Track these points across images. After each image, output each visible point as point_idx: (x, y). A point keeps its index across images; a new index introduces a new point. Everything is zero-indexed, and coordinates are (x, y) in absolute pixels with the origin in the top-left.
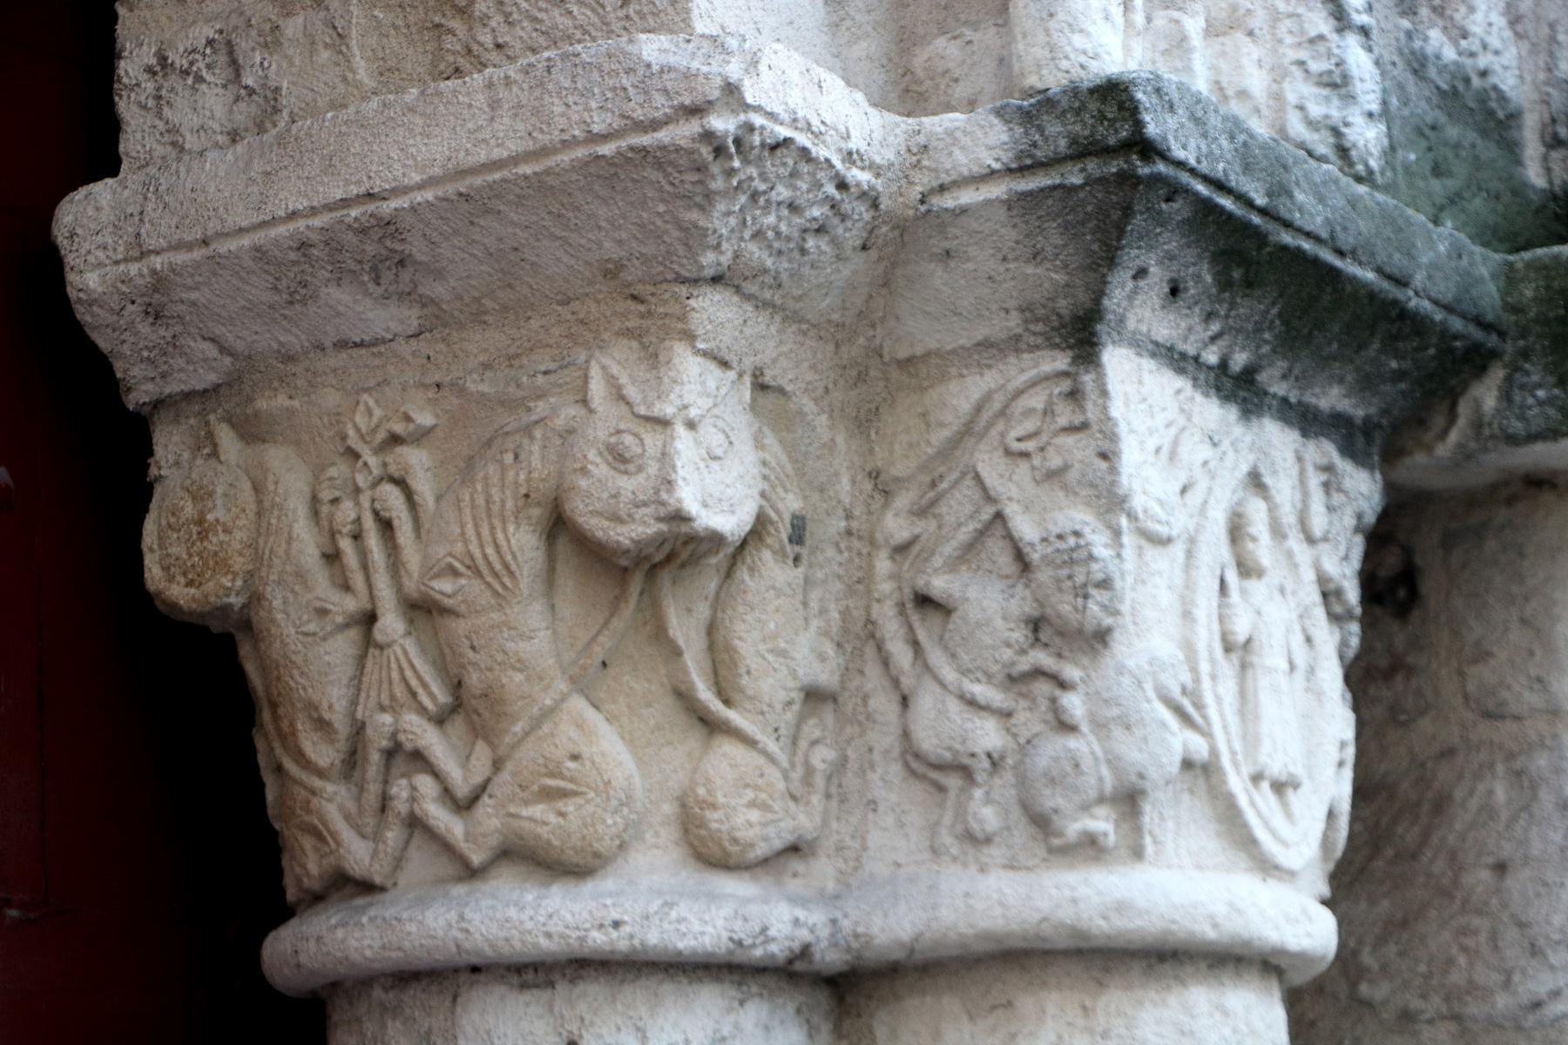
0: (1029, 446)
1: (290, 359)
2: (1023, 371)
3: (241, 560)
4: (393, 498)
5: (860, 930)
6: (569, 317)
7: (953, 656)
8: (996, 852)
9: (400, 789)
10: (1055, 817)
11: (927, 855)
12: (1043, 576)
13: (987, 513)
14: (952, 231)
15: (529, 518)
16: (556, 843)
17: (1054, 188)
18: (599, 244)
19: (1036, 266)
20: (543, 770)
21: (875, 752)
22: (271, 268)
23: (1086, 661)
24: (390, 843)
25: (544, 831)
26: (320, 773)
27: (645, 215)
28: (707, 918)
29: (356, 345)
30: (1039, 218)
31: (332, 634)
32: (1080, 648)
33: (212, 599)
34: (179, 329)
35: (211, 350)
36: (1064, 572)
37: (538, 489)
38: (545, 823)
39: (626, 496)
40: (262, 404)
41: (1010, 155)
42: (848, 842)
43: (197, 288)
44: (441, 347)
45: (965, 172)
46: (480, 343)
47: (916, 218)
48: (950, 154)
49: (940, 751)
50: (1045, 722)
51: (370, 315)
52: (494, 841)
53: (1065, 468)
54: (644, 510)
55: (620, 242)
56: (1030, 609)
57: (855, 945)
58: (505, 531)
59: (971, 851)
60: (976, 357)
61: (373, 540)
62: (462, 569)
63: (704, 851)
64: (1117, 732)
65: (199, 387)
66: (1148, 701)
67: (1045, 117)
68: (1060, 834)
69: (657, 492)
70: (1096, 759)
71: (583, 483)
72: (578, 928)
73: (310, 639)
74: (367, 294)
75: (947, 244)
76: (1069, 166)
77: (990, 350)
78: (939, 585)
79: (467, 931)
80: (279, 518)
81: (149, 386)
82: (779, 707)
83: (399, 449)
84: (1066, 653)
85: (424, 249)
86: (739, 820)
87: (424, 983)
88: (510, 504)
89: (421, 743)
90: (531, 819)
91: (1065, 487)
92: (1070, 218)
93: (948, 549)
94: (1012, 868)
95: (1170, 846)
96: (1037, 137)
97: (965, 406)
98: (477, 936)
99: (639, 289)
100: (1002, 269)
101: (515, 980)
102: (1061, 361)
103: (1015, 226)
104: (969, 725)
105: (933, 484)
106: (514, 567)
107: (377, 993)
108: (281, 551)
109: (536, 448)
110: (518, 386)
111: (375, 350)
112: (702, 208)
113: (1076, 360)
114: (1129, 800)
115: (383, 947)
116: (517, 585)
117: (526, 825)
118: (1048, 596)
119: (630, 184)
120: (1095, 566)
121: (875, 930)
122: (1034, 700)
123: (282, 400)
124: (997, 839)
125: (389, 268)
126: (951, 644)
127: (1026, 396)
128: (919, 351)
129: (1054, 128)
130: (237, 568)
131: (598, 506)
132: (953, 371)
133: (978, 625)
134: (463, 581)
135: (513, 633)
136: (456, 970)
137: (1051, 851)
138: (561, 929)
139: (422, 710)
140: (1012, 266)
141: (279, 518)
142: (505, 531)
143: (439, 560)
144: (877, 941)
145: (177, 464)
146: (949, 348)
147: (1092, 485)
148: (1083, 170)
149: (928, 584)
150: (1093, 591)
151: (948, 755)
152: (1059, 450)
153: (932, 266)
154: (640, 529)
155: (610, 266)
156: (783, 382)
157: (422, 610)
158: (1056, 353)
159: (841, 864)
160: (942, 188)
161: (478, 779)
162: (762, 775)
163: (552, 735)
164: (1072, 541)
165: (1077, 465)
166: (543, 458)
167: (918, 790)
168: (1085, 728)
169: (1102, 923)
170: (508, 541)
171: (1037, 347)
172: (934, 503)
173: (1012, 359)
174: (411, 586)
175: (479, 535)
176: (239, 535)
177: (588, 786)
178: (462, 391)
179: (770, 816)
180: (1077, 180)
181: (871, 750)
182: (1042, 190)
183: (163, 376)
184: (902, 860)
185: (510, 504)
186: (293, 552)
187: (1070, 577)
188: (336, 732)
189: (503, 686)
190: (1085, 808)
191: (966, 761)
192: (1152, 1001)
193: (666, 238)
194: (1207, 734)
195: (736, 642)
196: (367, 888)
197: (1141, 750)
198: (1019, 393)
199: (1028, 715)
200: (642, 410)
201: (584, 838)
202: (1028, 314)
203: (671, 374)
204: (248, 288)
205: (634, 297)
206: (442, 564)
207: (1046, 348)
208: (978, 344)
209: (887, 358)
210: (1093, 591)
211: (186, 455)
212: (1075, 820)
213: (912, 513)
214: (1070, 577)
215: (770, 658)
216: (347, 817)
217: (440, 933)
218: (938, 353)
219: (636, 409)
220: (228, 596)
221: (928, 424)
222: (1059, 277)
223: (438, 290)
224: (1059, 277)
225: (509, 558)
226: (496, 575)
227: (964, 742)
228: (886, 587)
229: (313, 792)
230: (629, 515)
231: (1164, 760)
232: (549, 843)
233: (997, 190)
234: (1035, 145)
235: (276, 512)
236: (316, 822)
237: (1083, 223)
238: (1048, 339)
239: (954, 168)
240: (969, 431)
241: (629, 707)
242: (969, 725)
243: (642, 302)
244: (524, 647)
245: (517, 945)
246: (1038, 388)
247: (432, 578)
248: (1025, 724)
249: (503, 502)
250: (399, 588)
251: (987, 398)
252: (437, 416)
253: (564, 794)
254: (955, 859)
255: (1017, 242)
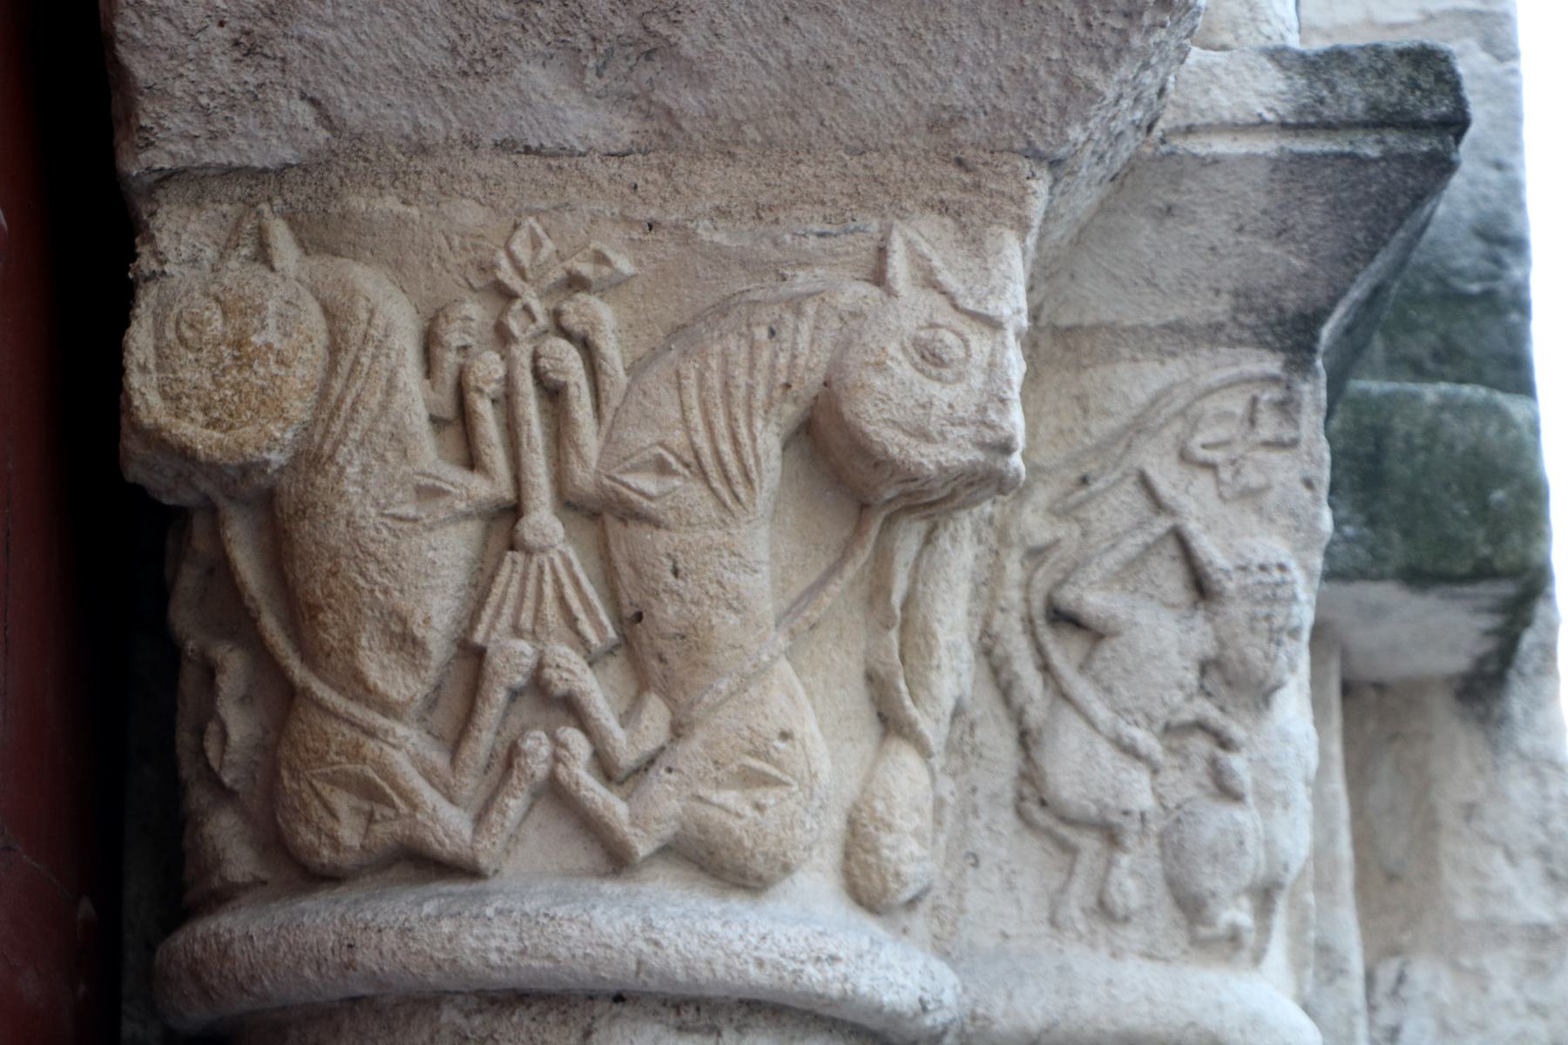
0: (1217, 456)
1: (423, 150)
2: (1216, 367)
3: (298, 404)
4: (568, 362)
5: (980, 1010)
6: (861, 171)
7: (1108, 690)
8: (1132, 935)
9: (537, 746)
10: (1211, 902)
11: (1045, 929)
12: (1237, 611)
13: (1162, 525)
14: (1188, 183)
15: (779, 415)
16: (748, 843)
17: (1341, 156)
18: (946, 83)
19: (1276, 246)
20: (747, 746)
21: (979, 794)
22: (462, 21)
23: (1248, 721)
24: (511, 814)
25: (735, 824)
26: (387, 708)
27: (1028, 58)
29: (527, 150)
30: (1306, 188)
31: (443, 523)
32: (1246, 706)
33: (249, 450)
34: (275, 75)
35: (305, 114)
36: (1263, 610)
37: (802, 380)
38: (739, 816)
39: (940, 408)
40: (357, 202)
41: (1288, 106)
42: (946, 901)
43: (334, 26)
44: (654, 175)
45: (1227, 116)
46: (714, 181)
47: (1153, 159)
48: (1207, 92)
49: (1085, 802)
50: (1200, 786)
51: (570, 114)
52: (667, 831)
53: (1267, 488)
54: (963, 431)
55: (975, 87)
56: (1209, 648)
57: (970, 1029)
58: (750, 426)
59: (1101, 929)
60: (1158, 340)
61: (531, 408)
62: (676, 465)
63: (861, 882)
65: (257, 164)
67: (1337, 72)
68: (1210, 923)
69: (982, 409)
71: (878, 382)
72: (794, 959)
73: (406, 526)
74: (580, 85)
75: (1173, 198)
76: (1359, 134)
77: (1181, 336)
78: (1093, 600)
79: (657, 943)
80: (374, 358)
81: (183, 148)
83: (582, 297)
84: (1230, 708)
85: (701, 41)
87: (535, 1009)
88: (761, 392)
89: (577, 686)
90: (721, 807)
91: (1259, 511)
92: (1344, 195)
93: (1111, 561)
94: (1150, 957)
96: (1325, 93)
97: (1140, 397)
98: (671, 951)
99: (969, 153)
100: (1231, 240)
101: (672, 1019)
102: (1272, 364)
103: (1270, 192)
104: (1123, 776)
105: (1084, 481)
106: (754, 475)
107: (449, 1015)
108: (374, 402)
109: (805, 327)
110: (776, 244)
111: (554, 163)
112: (1104, 67)
113: (1288, 365)
115: (523, 952)
116: (752, 500)
117: (716, 814)
118: (1235, 635)
119: (1031, 14)
121: (997, 1013)
122: (1187, 758)
123: (391, 203)
124: (1135, 919)
125: (627, 58)
126: (1105, 675)
127: (1215, 397)
128: (1089, 319)
129: (1348, 87)
130: (292, 413)
131: (898, 416)
132: (1125, 352)
133: (1150, 657)
134: (677, 482)
135: (735, 560)
136: (591, 997)
137: (1196, 942)
138: (776, 956)
139: (581, 641)
140: (1244, 239)
141: (374, 358)
142: (750, 426)
143: (642, 449)
144: (996, 1027)
145: (194, 261)
146: (1127, 323)
147: (1293, 514)
148: (1381, 142)
149: (1079, 599)
151: (1093, 809)
152: (1259, 467)
153: (1142, 221)
154: (953, 454)
155: (946, 116)
157: (599, 513)
158: (1264, 353)
159: (935, 926)
160: (1190, 130)
161: (649, 746)
163: (762, 702)
164: (1277, 575)
165: (1278, 489)
166: (813, 341)
167: (1033, 848)
168: (1250, 799)
170: (754, 439)
171: (1241, 342)
172: (1081, 504)
173: (1204, 351)
174: (585, 476)
175: (710, 426)
176: (300, 371)
177: (793, 776)
178: (685, 236)
180: (1371, 150)
181: (974, 790)
182: (1325, 155)
183: (214, 136)
184: (1011, 931)
185: (761, 392)
186: (396, 406)
187: (1268, 618)
188: (426, 654)
189: (712, 628)
191: (1115, 818)
193: (1041, 97)
195: (936, 625)
196: (461, 870)
198: (1210, 391)
199: (1178, 774)
200: (970, 305)
201: (780, 841)
202: (1242, 301)
203: (1003, 267)
204: (412, 40)
205: (960, 162)
206: (647, 455)
207: (1251, 345)
208: (1167, 326)
209: (1043, 322)
211: (210, 253)
213: (1051, 511)
214: (1268, 618)
216: (428, 774)
217: (618, 942)
218: (1112, 328)
219: (960, 302)
220: (269, 450)
221: (1085, 411)
222: (1299, 264)
223: (689, 101)
224: (1299, 264)
225: (751, 461)
226: (727, 479)
227: (1117, 796)
228: (1015, 595)
229: (371, 733)
230: (942, 433)
232: (739, 842)
233: (1267, 146)
234: (1321, 101)
235: (370, 349)
236: (371, 773)
237: (1357, 205)
238: (1256, 334)
239: (1212, 108)
240: (1139, 427)
241: (826, 683)
242: (1123, 776)
243: (967, 171)
244: (745, 581)
245: (720, 971)
246: (1234, 391)
247: (627, 471)
248: (1174, 785)
249: (751, 389)
250: (559, 478)
251: (1167, 392)
252: (639, 263)
253: (765, 780)
254: (1080, 937)
255: (1265, 212)
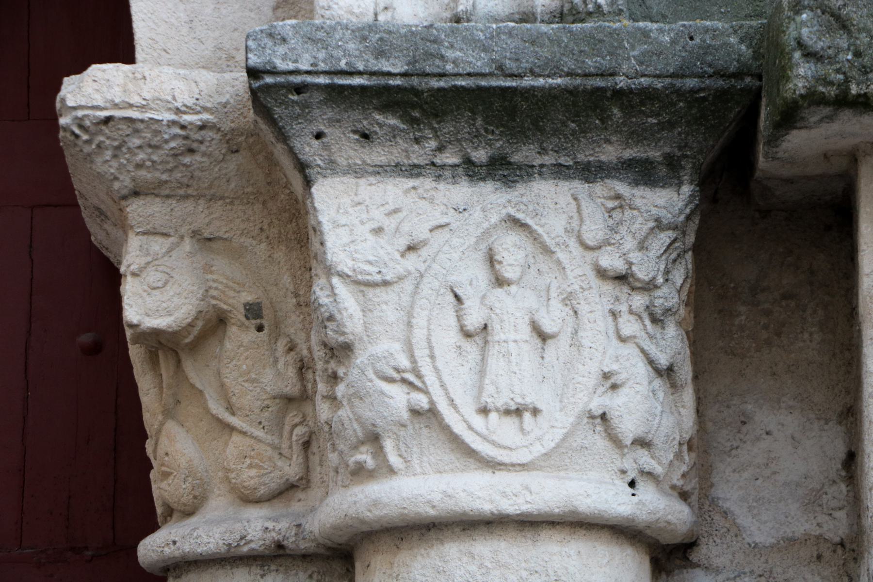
28: (211, 534)
64: (357, 402)
66: (371, 381)
70: (350, 419)
82: (257, 411)
86: (244, 476)
95: (415, 462)
114: (374, 439)
120: (323, 310)
150: (328, 324)
156: (221, 234)
162: (253, 450)
169: (369, 514)
179: (262, 471)
190: (355, 448)
192: (422, 555)
194: (426, 392)
197: (370, 410)
210: (328, 324)
212: (352, 456)
215: (246, 385)
231: (385, 414)
